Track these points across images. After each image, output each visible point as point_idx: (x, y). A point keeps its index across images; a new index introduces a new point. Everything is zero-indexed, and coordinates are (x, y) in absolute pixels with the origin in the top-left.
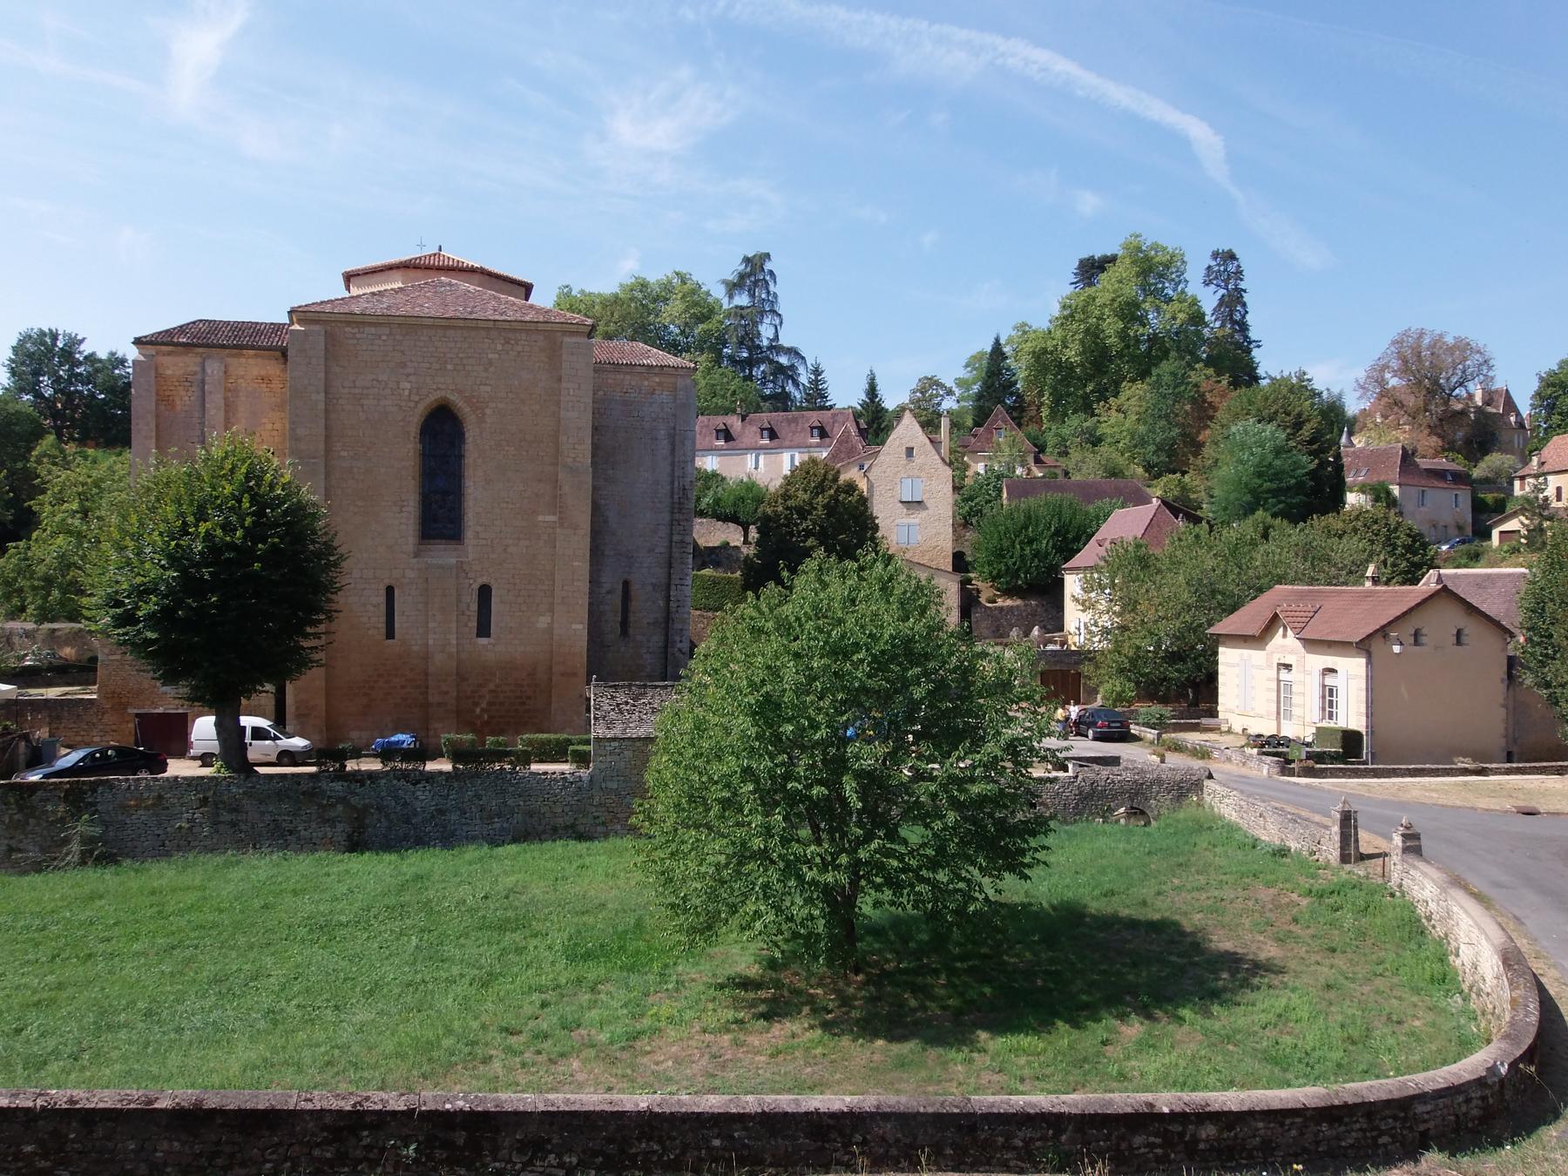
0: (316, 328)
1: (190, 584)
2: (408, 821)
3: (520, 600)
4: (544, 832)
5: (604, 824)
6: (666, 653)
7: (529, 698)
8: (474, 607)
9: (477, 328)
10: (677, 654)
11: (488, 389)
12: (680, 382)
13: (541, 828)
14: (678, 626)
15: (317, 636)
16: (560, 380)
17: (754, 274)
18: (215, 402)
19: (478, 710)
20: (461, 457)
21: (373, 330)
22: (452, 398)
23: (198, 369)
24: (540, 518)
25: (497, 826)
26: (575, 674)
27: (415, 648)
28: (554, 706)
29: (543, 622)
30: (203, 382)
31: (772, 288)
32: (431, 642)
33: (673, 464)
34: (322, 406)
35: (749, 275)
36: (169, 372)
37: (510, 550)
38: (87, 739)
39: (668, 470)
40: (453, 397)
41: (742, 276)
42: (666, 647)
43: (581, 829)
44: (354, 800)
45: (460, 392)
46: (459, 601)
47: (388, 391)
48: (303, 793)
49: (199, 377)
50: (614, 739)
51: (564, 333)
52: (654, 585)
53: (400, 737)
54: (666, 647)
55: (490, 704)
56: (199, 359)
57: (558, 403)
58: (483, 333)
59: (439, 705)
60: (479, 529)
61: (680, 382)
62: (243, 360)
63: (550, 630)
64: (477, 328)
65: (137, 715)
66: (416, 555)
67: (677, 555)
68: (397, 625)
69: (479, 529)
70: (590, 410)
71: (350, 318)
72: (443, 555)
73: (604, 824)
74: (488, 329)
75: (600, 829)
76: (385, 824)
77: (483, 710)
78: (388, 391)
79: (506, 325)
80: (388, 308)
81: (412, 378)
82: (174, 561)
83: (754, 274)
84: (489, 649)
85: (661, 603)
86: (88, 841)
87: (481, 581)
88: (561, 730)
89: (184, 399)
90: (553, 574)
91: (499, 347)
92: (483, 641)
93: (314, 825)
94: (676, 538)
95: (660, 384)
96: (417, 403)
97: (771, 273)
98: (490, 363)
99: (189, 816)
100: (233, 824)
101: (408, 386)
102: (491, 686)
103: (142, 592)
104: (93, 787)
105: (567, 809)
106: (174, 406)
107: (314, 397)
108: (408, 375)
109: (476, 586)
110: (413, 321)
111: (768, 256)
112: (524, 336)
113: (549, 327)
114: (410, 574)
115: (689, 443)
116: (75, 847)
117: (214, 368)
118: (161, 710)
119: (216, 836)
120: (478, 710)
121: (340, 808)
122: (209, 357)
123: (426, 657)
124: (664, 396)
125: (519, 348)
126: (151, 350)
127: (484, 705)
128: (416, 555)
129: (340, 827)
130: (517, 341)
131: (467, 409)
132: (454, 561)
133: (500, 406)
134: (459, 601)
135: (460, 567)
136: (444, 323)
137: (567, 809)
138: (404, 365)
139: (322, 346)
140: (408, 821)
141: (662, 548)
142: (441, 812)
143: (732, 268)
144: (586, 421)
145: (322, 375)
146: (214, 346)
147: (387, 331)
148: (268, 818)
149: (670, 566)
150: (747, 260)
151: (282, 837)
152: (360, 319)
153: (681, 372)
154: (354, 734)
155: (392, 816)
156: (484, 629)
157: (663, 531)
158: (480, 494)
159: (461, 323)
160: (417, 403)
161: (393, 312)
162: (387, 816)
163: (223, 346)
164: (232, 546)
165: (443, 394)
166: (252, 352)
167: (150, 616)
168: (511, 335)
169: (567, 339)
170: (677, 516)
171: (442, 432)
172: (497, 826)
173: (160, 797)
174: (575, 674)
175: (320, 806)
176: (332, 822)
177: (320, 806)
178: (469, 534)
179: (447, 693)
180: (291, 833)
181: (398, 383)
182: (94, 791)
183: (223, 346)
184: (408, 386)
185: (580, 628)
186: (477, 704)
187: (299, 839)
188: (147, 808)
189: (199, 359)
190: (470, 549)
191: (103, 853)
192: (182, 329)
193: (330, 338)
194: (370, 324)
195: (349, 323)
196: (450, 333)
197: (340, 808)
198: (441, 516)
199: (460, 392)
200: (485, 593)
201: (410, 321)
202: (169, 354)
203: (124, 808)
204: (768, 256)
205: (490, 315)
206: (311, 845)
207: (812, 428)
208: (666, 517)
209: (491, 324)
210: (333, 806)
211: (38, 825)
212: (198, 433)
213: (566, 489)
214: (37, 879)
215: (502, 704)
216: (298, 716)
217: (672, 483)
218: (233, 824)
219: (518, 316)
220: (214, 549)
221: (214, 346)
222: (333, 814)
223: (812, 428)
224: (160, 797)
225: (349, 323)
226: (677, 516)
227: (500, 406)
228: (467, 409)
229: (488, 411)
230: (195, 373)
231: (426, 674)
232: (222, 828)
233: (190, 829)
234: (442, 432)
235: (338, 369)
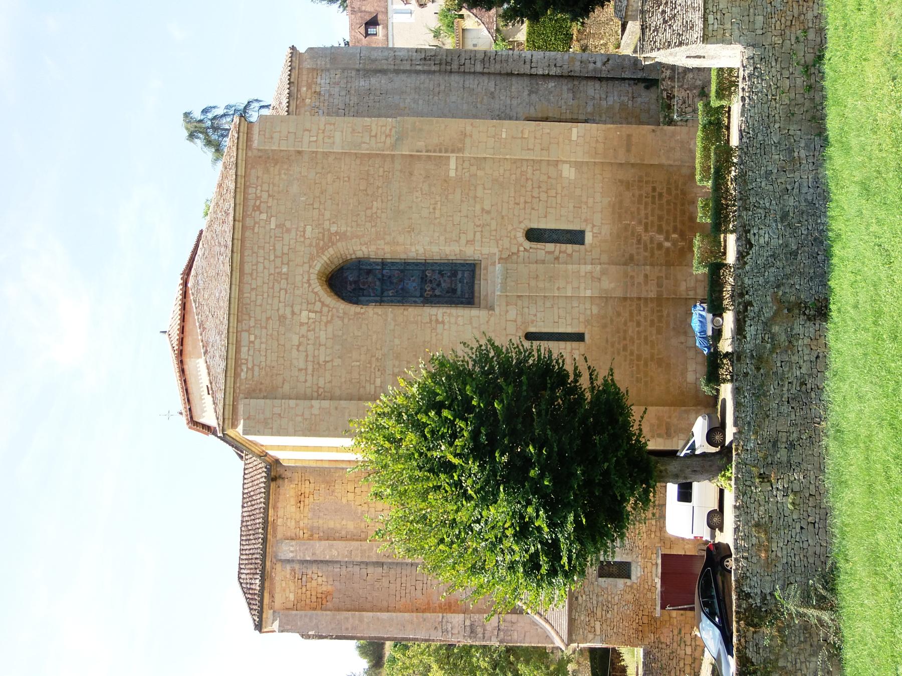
0: (241, 408)
1: (515, 477)
2: (794, 254)
3: (543, 196)
4: (812, 100)
5: (805, 31)
6: (608, 79)
7: (654, 189)
8: (550, 247)
9: (243, 240)
10: (608, 66)
11: (309, 228)
12: (307, 65)
13: (807, 103)
14: (577, 66)
15: (578, 375)
16: (299, 152)
17: (205, 130)
18: (322, 550)
19: (667, 244)
20: (384, 264)
21: (244, 350)
22: (318, 268)
23: (288, 567)
24: (452, 174)
25: (803, 154)
26: (629, 136)
27: (595, 310)
28: (664, 161)
29: (568, 172)
30: (303, 562)
31: (220, 112)
32: (588, 293)
33: (397, 72)
34: (326, 404)
35: (206, 134)
36: (292, 597)
37: (487, 208)
38: (689, 660)
39: (403, 77)
40: (318, 266)
41: (209, 143)
42: (600, 79)
43: (810, 58)
44: (768, 313)
45: (312, 259)
46: (543, 262)
47: (311, 335)
48: (758, 369)
49: (297, 566)
50: (705, 20)
51: (248, 147)
52: (531, 93)
53: (695, 324)
54: (600, 79)
55: (660, 230)
56: (279, 566)
57: (326, 155)
58: (248, 234)
59: (659, 285)
60: (463, 241)
61: (307, 65)
62: (280, 522)
63: (578, 165)
64: (243, 240)
65: (663, 607)
66: (492, 308)
67: (498, 66)
68: (569, 330)
69: (463, 241)
70: (332, 119)
71: (231, 373)
72: (491, 283)
73: (805, 31)
74: (244, 228)
75: (811, 35)
76: (796, 279)
77: (667, 239)
78: (311, 335)
79: (240, 209)
80: (220, 333)
81: (297, 309)
82: (488, 498)
83: (205, 130)
84: (598, 231)
85: (551, 84)
86: (806, 600)
87: (521, 238)
88: (692, 153)
89: (320, 581)
90: (515, 161)
91: (264, 216)
92: (589, 238)
93: (795, 358)
94: (479, 68)
95: (309, 87)
96: (323, 304)
97: (205, 111)
98: (279, 226)
99: (780, 494)
100: (791, 446)
101: (305, 314)
102: (640, 229)
103: (524, 531)
104: (744, 596)
105: (786, 74)
106: (328, 594)
107: (316, 411)
108: (293, 313)
109: (527, 244)
110: (234, 305)
111: (187, 115)
112: (251, 190)
113: (242, 164)
114: (512, 314)
115: (375, 55)
116: (812, 613)
117: (287, 550)
118: (658, 581)
119: (804, 466)
120: (667, 244)
121: (776, 329)
122: (276, 556)
123: (606, 299)
124: (323, 81)
125: (265, 195)
126: (268, 614)
127: (661, 238)
128: (492, 308)
129: (798, 329)
130: (257, 198)
131: (331, 251)
132: (498, 267)
133: (327, 215)
134: (543, 262)
135: (507, 259)
136: (236, 274)
137: (786, 74)
138: (282, 319)
139: (261, 402)
140: (794, 254)
141: (489, 84)
142: (784, 216)
143: (200, 152)
144: (345, 123)
145: (292, 403)
146: (264, 549)
147: (245, 335)
148: (785, 409)
149: (511, 74)
150: (192, 136)
151: (807, 394)
152: (232, 363)
153: (296, 64)
154: (690, 377)
155: (788, 270)
156: (575, 237)
157: (471, 82)
158: (423, 241)
159: (237, 257)
160: (323, 304)
161: (224, 328)
162: (787, 277)
163: (265, 540)
164: (475, 435)
165: (314, 277)
166: (271, 512)
167: (552, 525)
168: (251, 203)
169: (255, 144)
170: (455, 67)
171: (354, 281)
172: (803, 154)
173: (757, 525)
174: (629, 136)
175: (772, 350)
176: (792, 338)
177: (772, 350)
178: (470, 253)
179: (646, 276)
180: (804, 383)
181: (302, 324)
182: (748, 596)
183: (265, 540)
184: (305, 314)
185: (576, 131)
186: (660, 246)
187: (810, 375)
188: (770, 540)
189: (279, 566)
190: (485, 251)
191: (824, 586)
192: (246, 590)
193: (251, 394)
194: (238, 351)
195: (236, 375)
196: (247, 268)
197: (776, 329)
198: (450, 284)
199: (312, 259)
200: (534, 235)
201: (234, 310)
202: (272, 596)
203: (770, 563)
204: (187, 115)
205: (228, 227)
206: (820, 361)
207: (367, 35)
208: (455, 79)
209: (239, 225)
210: (773, 337)
211: (785, 656)
212: (357, 569)
213: (421, 144)
214: (848, 654)
215: (660, 218)
216: (668, 435)
217: (418, 72)
218: (791, 446)
219: (230, 196)
220: (480, 451)
221: (264, 549)
222: (783, 337)
223: (367, 35)
224: (757, 525)
225: (236, 375)
226: (455, 67)
227: (327, 215)
228: (331, 251)
229: (334, 229)
230: (293, 570)
231: (625, 299)
232: (794, 460)
233: (795, 493)
234: (354, 281)
235: (287, 387)
